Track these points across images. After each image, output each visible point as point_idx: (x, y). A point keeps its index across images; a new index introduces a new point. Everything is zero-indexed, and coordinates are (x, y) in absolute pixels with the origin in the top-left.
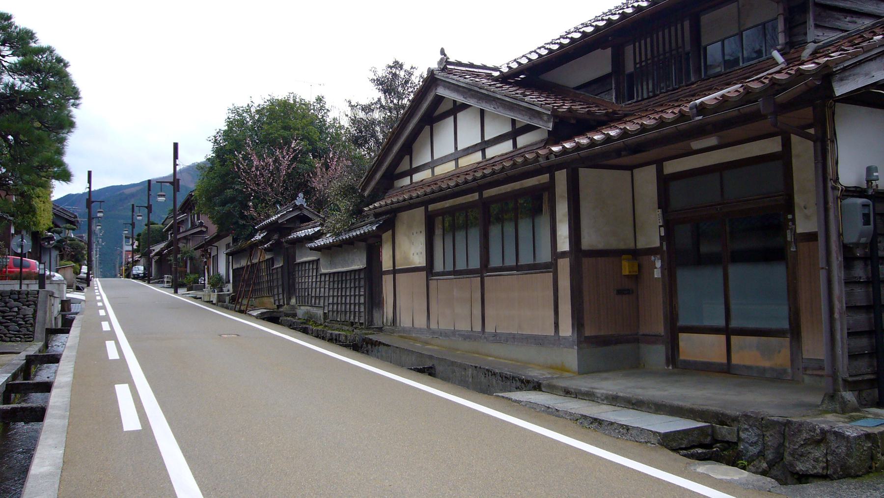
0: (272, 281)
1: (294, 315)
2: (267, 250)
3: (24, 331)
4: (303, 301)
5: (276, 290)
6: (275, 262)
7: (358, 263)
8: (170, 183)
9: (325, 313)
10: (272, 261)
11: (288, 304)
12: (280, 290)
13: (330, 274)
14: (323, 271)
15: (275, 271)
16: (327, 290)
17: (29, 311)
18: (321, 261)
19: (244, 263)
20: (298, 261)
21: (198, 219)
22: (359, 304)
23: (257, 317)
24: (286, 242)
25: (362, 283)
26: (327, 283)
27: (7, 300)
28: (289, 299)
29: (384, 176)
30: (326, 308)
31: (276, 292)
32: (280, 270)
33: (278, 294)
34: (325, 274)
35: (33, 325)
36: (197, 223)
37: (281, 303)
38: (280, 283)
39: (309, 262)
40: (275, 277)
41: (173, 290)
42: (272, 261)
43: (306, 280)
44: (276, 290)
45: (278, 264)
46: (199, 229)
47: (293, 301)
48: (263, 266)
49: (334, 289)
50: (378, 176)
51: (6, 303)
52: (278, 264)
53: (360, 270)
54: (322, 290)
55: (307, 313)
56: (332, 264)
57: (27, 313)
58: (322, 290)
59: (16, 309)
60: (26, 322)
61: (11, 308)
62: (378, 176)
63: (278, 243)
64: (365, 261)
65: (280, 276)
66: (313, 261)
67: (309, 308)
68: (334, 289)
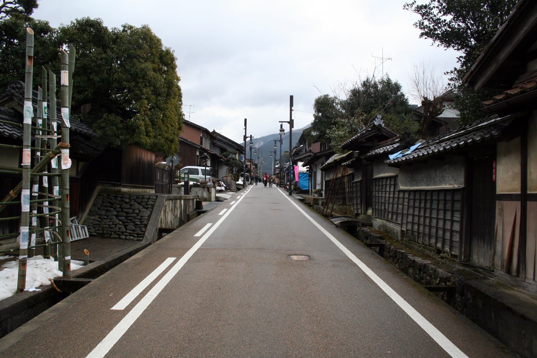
0: (352, 192)
1: (371, 225)
2: (348, 166)
3: (138, 230)
4: (381, 214)
5: (355, 201)
6: (356, 177)
7: (452, 181)
8: (288, 122)
9: (402, 231)
10: (352, 176)
11: (365, 213)
12: (359, 201)
13: (410, 192)
14: (402, 187)
15: (354, 185)
16: (406, 207)
17: (146, 213)
18: (399, 179)
19: (331, 177)
20: (376, 176)
21: (309, 148)
22: (452, 231)
23: (337, 226)
24: (365, 159)
25: (458, 206)
26: (406, 200)
27: (133, 202)
28: (366, 210)
29: (512, 56)
30: (404, 226)
31: (355, 203)
32: (358, 184)
33: (357, 204)
34: (404, 191)
35: (146, 226)
36: (308, 149)
37: (360, 212)
38: (359, 195)
39: (386, 178)
40: (355, 189)
41: (288, 193)
42: (352, 176)
43: (384, 195)
44: (355, 201)
45: (358, 179)
46: (309, 154)
47: (370, 212)
48: (346, 180)
49: (414, 207)
50: (503, 55)
51: (131, 206)
52: (358, 179)
53: (453, 191)
54: (400, 206)
55: (383, 226)
56: (413, 181)
57: (144, 214)
58: (400, 206)
59: (137, 211)
60: (141, 222)
61: (134, 210)
62: (503, 55)
63: (358, 160)
64: (462, 180)
65: (359, 189)
66: (390, 178)
67: (385, 222)
68: (414, 207)
